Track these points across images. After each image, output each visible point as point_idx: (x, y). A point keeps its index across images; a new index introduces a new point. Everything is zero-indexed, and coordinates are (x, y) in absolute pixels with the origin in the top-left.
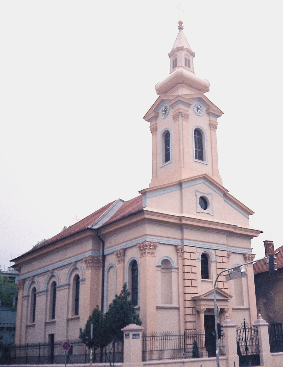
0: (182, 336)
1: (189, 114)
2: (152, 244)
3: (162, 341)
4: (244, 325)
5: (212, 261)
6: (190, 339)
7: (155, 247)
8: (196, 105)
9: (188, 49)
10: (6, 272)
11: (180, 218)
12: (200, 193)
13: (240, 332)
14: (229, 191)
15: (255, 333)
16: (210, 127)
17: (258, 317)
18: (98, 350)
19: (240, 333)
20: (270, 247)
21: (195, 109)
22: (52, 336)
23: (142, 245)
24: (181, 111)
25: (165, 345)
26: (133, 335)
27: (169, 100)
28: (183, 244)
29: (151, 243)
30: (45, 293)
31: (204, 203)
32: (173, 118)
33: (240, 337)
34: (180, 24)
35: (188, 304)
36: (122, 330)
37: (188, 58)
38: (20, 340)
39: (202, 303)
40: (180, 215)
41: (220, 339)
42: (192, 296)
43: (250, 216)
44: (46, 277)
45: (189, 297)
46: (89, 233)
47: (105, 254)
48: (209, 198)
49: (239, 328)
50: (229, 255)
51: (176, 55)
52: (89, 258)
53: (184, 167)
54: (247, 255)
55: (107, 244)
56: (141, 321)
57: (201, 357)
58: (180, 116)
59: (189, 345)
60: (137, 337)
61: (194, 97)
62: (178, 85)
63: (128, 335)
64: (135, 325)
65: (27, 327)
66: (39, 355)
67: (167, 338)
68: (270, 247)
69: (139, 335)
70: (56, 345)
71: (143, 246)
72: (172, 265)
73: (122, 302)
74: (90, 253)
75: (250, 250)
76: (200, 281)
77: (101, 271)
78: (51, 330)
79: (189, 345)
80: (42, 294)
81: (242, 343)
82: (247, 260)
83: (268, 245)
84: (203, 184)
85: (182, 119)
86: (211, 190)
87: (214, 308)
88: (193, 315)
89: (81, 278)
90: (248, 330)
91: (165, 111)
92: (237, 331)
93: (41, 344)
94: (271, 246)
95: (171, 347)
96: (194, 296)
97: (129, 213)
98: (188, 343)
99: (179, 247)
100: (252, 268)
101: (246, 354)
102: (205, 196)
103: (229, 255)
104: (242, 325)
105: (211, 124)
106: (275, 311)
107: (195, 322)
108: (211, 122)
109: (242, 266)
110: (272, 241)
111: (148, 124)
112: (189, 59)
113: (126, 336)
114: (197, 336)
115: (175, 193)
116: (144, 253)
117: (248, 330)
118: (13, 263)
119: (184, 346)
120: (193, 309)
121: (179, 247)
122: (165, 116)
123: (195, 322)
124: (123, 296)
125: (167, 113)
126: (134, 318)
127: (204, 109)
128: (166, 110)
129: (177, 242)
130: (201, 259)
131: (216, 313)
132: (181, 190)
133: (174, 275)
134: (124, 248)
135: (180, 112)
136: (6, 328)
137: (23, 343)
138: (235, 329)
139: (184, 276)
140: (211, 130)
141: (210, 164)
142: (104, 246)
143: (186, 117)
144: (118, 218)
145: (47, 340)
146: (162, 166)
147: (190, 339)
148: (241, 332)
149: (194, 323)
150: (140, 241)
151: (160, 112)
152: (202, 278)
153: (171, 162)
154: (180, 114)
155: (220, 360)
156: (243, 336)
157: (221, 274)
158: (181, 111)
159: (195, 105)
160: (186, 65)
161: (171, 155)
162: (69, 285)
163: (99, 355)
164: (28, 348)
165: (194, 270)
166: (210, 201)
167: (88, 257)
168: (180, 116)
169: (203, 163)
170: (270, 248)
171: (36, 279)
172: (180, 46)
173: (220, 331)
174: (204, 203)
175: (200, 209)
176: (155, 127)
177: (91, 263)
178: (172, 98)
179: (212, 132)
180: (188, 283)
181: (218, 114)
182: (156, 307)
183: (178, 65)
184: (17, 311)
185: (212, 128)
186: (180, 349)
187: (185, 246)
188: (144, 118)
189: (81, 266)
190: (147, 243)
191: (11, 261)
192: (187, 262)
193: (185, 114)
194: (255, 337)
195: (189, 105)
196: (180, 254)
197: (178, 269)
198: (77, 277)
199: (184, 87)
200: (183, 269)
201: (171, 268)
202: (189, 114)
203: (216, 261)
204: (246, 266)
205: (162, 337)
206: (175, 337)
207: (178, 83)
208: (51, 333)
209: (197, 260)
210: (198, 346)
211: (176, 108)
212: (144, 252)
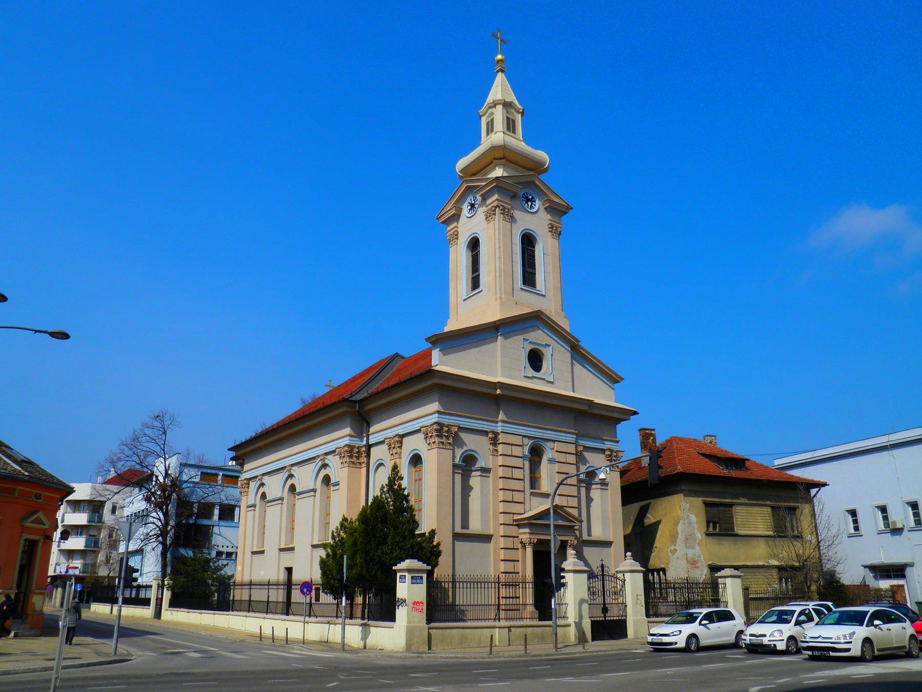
3: (469, 590)
4: (600, 569)
10: (227, 468)
14: (580, 342)
17: (626, 556)
19: (594, 583)
21: (523, 200)
22: (289, 570)
23: (429, 429)
25: (472, 596)
26: (412, 578)
27: (478, 186)
31: (535, 359)
36: (394, 568)
37: (511, 117)
44: (282, 476)
51: (492, 114)
66: (454, 575)
67: (469, 586)
69: (422, 578)
70: (295, 585)
77: (364, 470)
78: (288, 560)
81: (597, 599)
83: (646, 436)
87: (215, 552)
89: (332, 481)
90: (607, 579)
93: (236, 584)
94: (652, 438)
101: (603, 619)
102: (538, 349)
109: (601, 468)
110: (654, 430)
112: (514, 118)
113: (400, 578)
114: (521, 584)
117: (607, 579)
118: (232, 454)
119: (497, 600)
122: (472, 214)
125: (476, 208)
134: (401, 434)
136: (857, 525)
137: (246, 579)
144: (391, 383)
145: (282, 577)
146: (466, 297)
147: (508, 589)
153: (481, 291)
154: (497, 209)
155: (559, 626)
156: (600, 588)
157: (563, 483)
159: (524, 194)
161: (481, 278)
163: (360, 607)
174: (535, 359)
175: (531, 372)
176: (456, 233)
177: (348, 456)
178: (484, 184)
183: (495, 130)
188: (640, 430)
189: (333, 460)
207: (495, 159)
212: (433, 441)
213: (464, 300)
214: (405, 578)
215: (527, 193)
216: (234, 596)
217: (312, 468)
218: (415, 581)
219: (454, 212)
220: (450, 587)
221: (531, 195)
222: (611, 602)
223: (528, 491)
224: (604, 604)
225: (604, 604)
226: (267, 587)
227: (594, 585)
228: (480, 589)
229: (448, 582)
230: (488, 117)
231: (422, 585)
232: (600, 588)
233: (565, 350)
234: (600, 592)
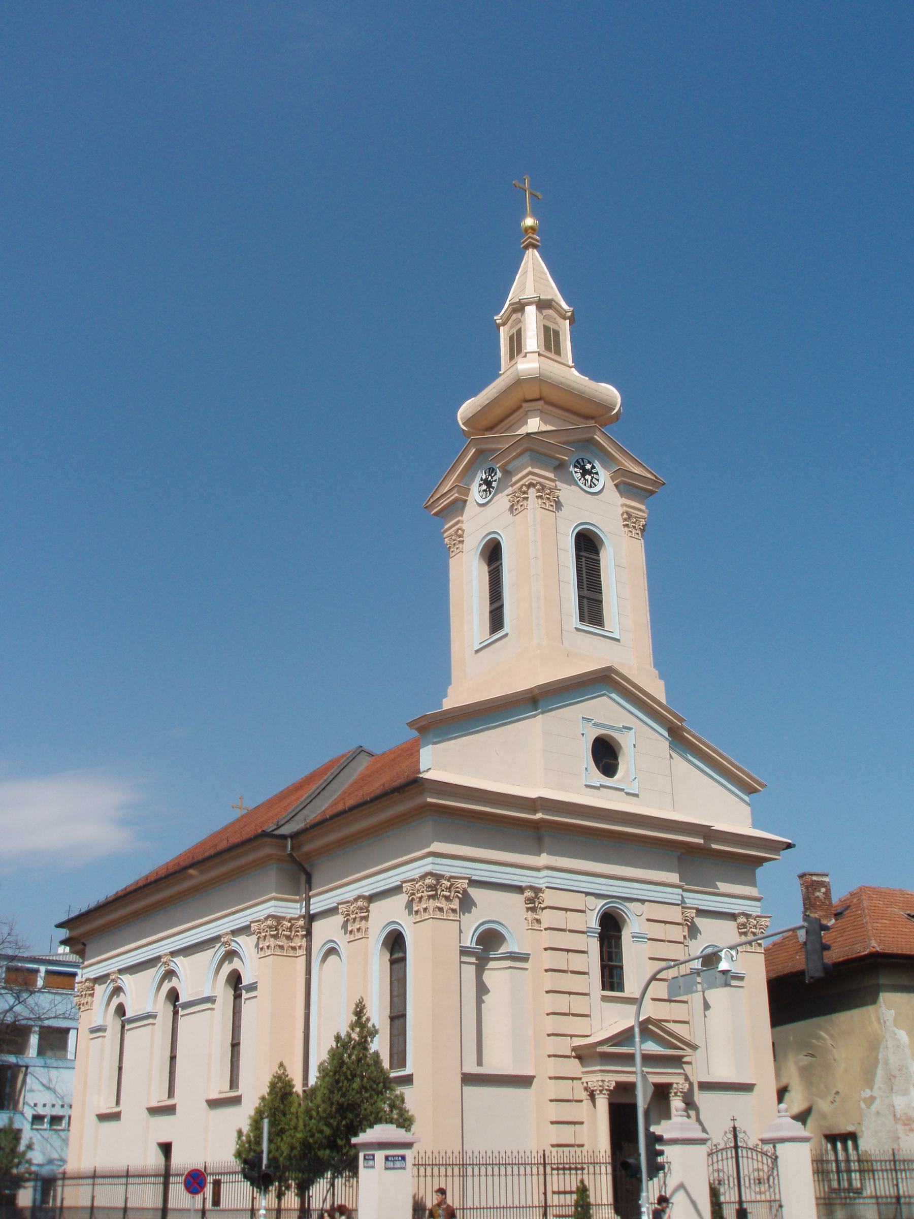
0: (731, 1151)
4: (731, 1136)
6: (567, 1177)
13: (720, 1158)
18: (291, 1200)
19: (720, 1163)
20: (818, 894)
21: (576, 472)
24: (535, 482)
33: (721, 1174)
36: (354, 1140)
37: (552, 326)
38: (880, 1193)
41: (655, 1180)
46: (267, 850)
47: (312, 912)
48: (626, 742)
49: (715, 1145)
56: (410, 1114)
60: (398, 1164)
62: (525, 405)
63: (370, 1158)
64: (393, 1127)
68: (818, 894)
73: (354, 1057)
90: (745, 1155)
92: (710, 1154)
93: (67, 1176)
97: (382, 787)
100: (761, 958)
104: (725, 1139)
106: (837, 1093)
112: (556, 328)
113: (365, 1159)
124: (357, 1039)
126: (392, 1107)
130: (599, 929)
131: (642, 1102)
138: (703, 1150)
148: (722, 1160)
152: (603, 989)
156: (731, 1172)
164: (131, 1180)
170: (818, 897)
173: (653, 1154)
175: (598, 778)
182: (463, 1074)
183: (524, 351)
184: (765, 980)
191: (60, 926)
198: (235, 980)
204: (734, 953)
205: (436, 1169)
206: (528, 1168)
207: (527, 401)
210: (249, 1183)
214: (373, 1159)
216: (62, 1199)
218: (390, 1164)
220: (608, 1172)
222: (753, 1199)
223: (597, 990)
224: (741, 1202)
225: (741, 1202)
226: (124, 1180)
227: (721, 1167)
230: (511, 328)
232: (731, 1172)
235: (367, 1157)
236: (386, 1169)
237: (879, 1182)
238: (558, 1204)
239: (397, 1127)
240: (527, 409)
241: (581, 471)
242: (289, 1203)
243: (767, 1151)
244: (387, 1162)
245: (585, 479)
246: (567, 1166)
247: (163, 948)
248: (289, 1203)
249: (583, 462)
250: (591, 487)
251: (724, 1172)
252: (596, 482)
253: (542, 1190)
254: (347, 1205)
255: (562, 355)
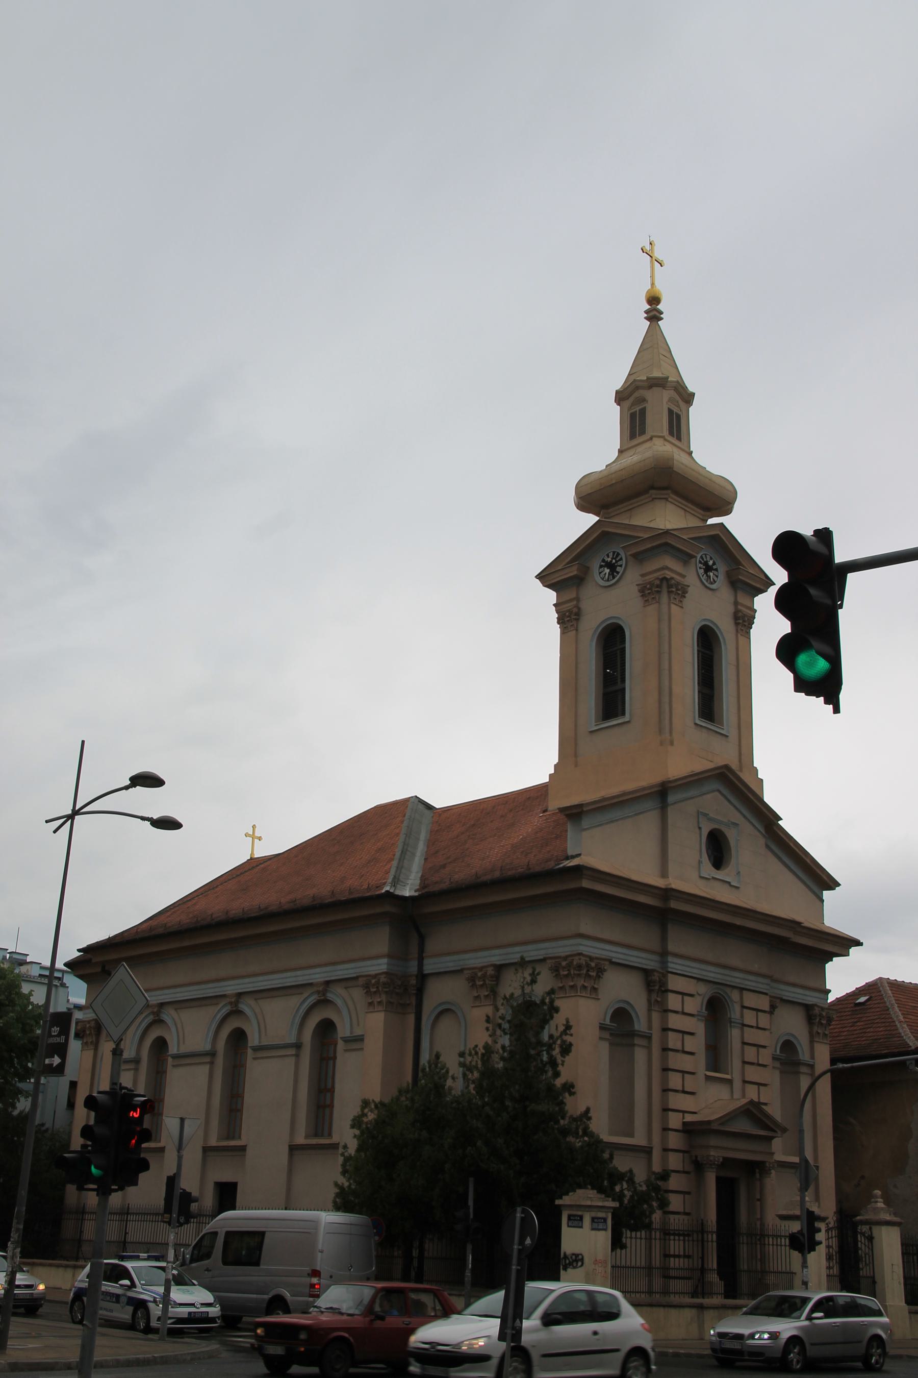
1: (686, 583)
2: (593, 964)
5: (731, 1022)
7: (600, 971)
8: (704, 556)
9: (678, 382)
11: (667, 893)
12: (711, 820)
14: (781, 819)
15: (867, 1244)
16: (737, 624)
21: (700, 568)
24: (668, 577)
26: (593, 1220)
28: (667, 967)
29: (591, 959)
30: (208, 1059)
32: (639, 591)
33: (831, 1250)
34: (650, 305)
35: (675, 1141)
36: (557, 1202)
37: (675, 410)
39: (713, 1141)
40: (660, 883)
42: (683, 1118)
43: (826, 894)
45: (675, 1121)
47: (426, 972)
48: (731, 835)
50: (773, 1007)
52: (383, 979)
53: (672, 743)
54: (817, 1011)
55: (431, 946)
57: (739, 1299)
58: (665, 590)
59: (675, 1256)
61: (701, 535)
65: (206, 1150)
69: (605, 1220)
71: (569, 965)
72: (636, 1027)
74: (381, 966)
75: (822, 996)
76: (702, 1078)
77: (411, 1018)
79: (675, 1256)
80: (197, 1060)
81: (865, 1269)
82: (653, 990)
84: (717, 794)
85: (669, 598)
86: (738, 814)
88: (684, 1172)
91: (612, 567)
95: (628, 1261)
96: (689, 1118)
98: (672, 1253)
99: (656, 977)
103: (773, 1007)
105: (740, 614)
106: (863, 1177)
107: (689, 1193)
108: (739, 607)
111: (551, 596)
112: (680, 413)
115: (648, 822)
116: (572, 987)
120: (685, 1154)
121: (656, 977)
123: (689, 1193)
127: (722, 568)
128: (614, 561)
129: (649, 962)
132: (664, 807)
133: (640, 1055)
135: (664, 579)
139: (664, 1059)
140: (737, 631)
141: (733, 733)
142: (421, 950)
143: (678, 591)
149: (687, 1196)
150: (562, 949)
151: (595, 565)
153: (628, 722)
154: (665, 584)
158: (669, 574)
159: (701, 557)
160: (671, 433)
162: (298, 1046)
164: (130, 1217)
165: (690, 1044)
166: (732, 843)
167: (375, 976)
168: (665, 590)
169: (712, 728)
171: (168, 1015)
172: (656, 374)
175: (708, 869)
176: (575, 610)
179: (742, 639)
180: (675, 1081)
181: (758, 586)
183: (649, 432)
185: (740, 627)
186: (649, 1268)
187: (669, 975)
188: (541, 577)
190: (583, 961)
192: (674, 1021)
193: (678, 584)
194: (865, 1255)
195: (686, 558)
196: (582, 982)
197: (649, 1038)
199: (670, 499)
200: (664, 1040)
201: (633, 1034)
202: (689, 586)
203: (741, 1022)
207: (653, 488)
208: (226, 1176)
209: (698, 1015)
211: (653, 565)
213: (591, 732)
215: (706, 555)
217: (293, 1005)
218: (595, 1225)
219: (575, 573)
220: (642, 1237)
221: (711, 558)
223: (702, 1071)
228: (634, 1240)
229: (712, 1232)
230: (633, 405)
231: (581, 1229)
233: (758, 833)
234: (867, 1256)
235: (572, 1218)
236: (593, 1229)
237: (712, 1239)
238: (678, 1267)
239: (597, 1192)
240: (654, 496)
241: (704, 567)
242: (133, 1225)
243: (864, 1232)
244: (594, 1224)
245: (707, 575)
246: (677, 1232)
247: (231, 988)
248: (133, 1225)
249: (706, 558)
250: (712, 583)
251: (833, 1248)
252: (715, 579)
253: (700, 1255)
254: (168, 1226)
255: (682, 440)
